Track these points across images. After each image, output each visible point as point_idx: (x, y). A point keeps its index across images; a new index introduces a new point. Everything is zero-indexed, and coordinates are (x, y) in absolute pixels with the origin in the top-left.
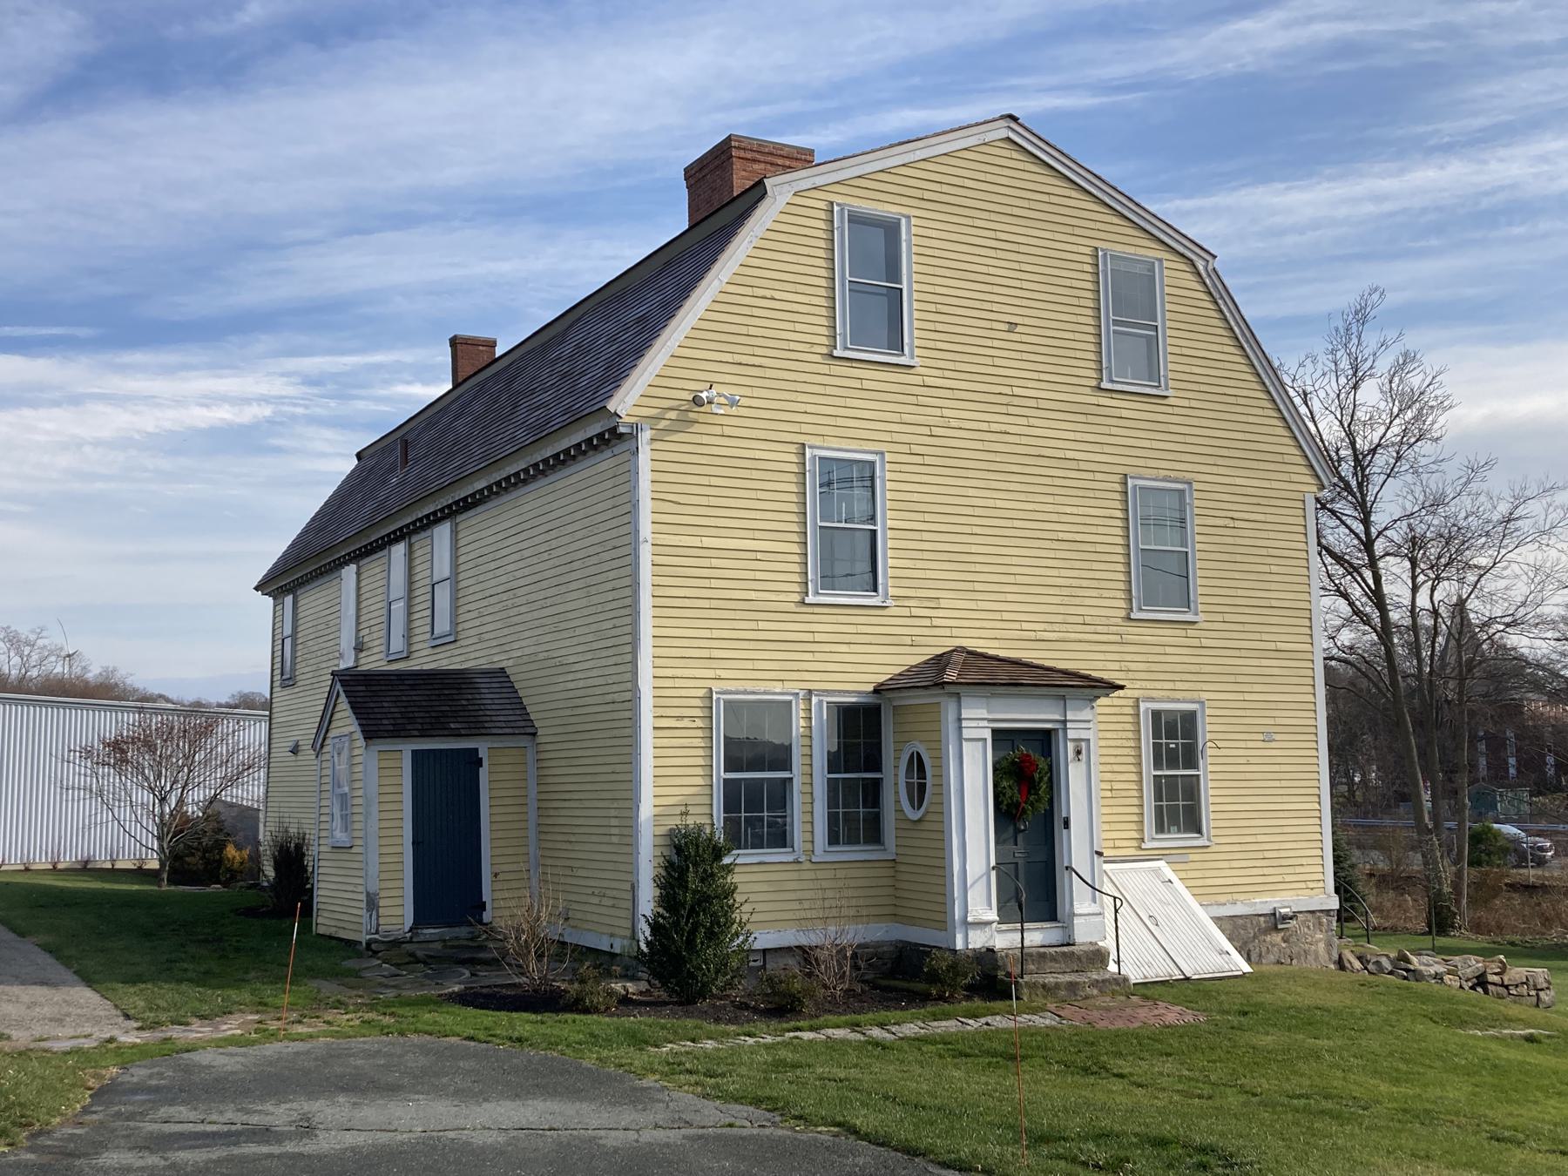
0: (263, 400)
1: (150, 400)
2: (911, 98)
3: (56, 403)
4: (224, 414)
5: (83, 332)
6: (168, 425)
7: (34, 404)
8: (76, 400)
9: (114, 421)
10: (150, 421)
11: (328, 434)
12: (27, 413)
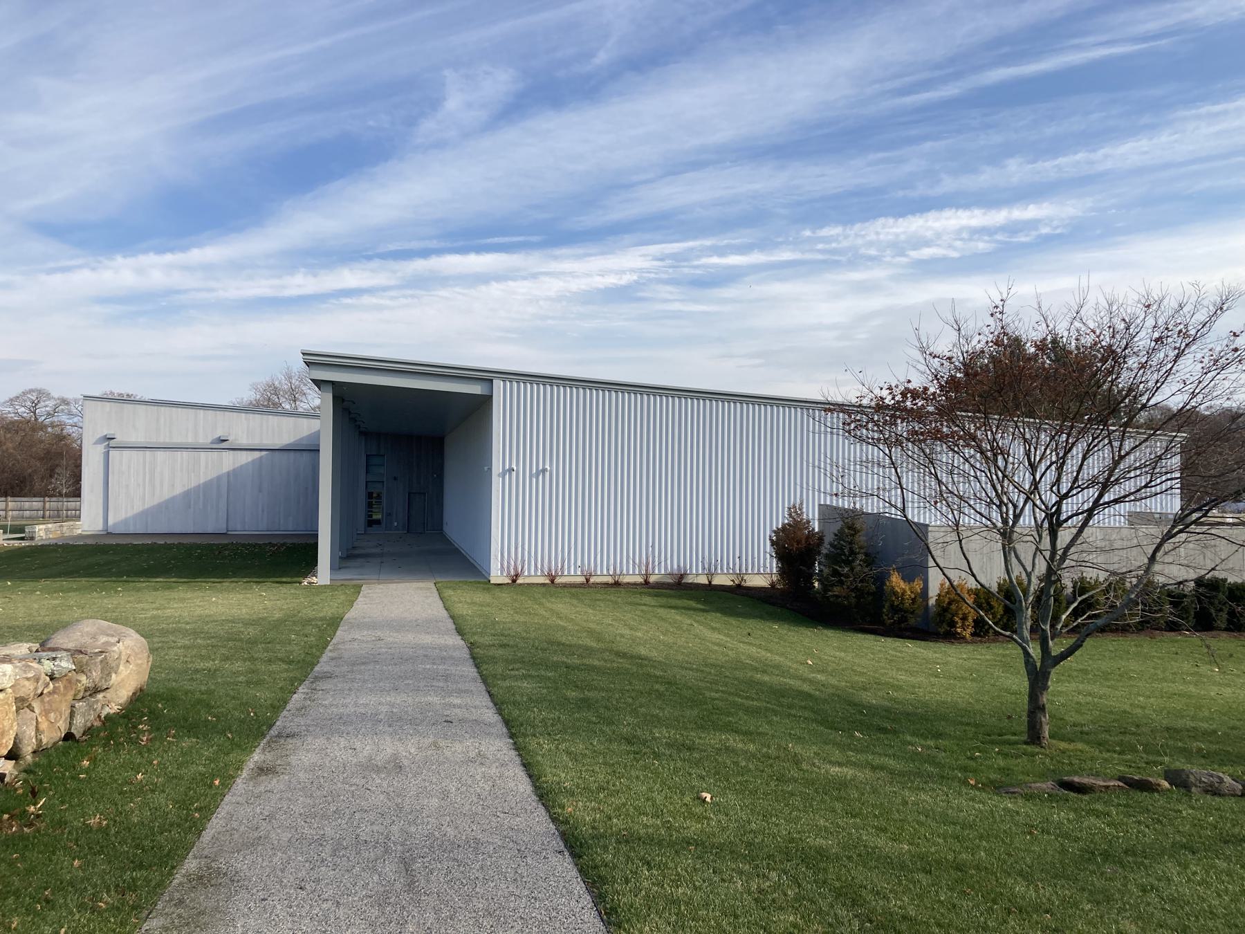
0: (633, 271)
1: (572, 274)
2: (1003, 61)
3: (525, 278)
4: (611, 280)
5: (534, 239)
6: (583, 287)
7: (514, 279)
8: (534, 276)
9: (554, 286)
10: (576, 285)
11: (669, 288)
12: (511, 283)
